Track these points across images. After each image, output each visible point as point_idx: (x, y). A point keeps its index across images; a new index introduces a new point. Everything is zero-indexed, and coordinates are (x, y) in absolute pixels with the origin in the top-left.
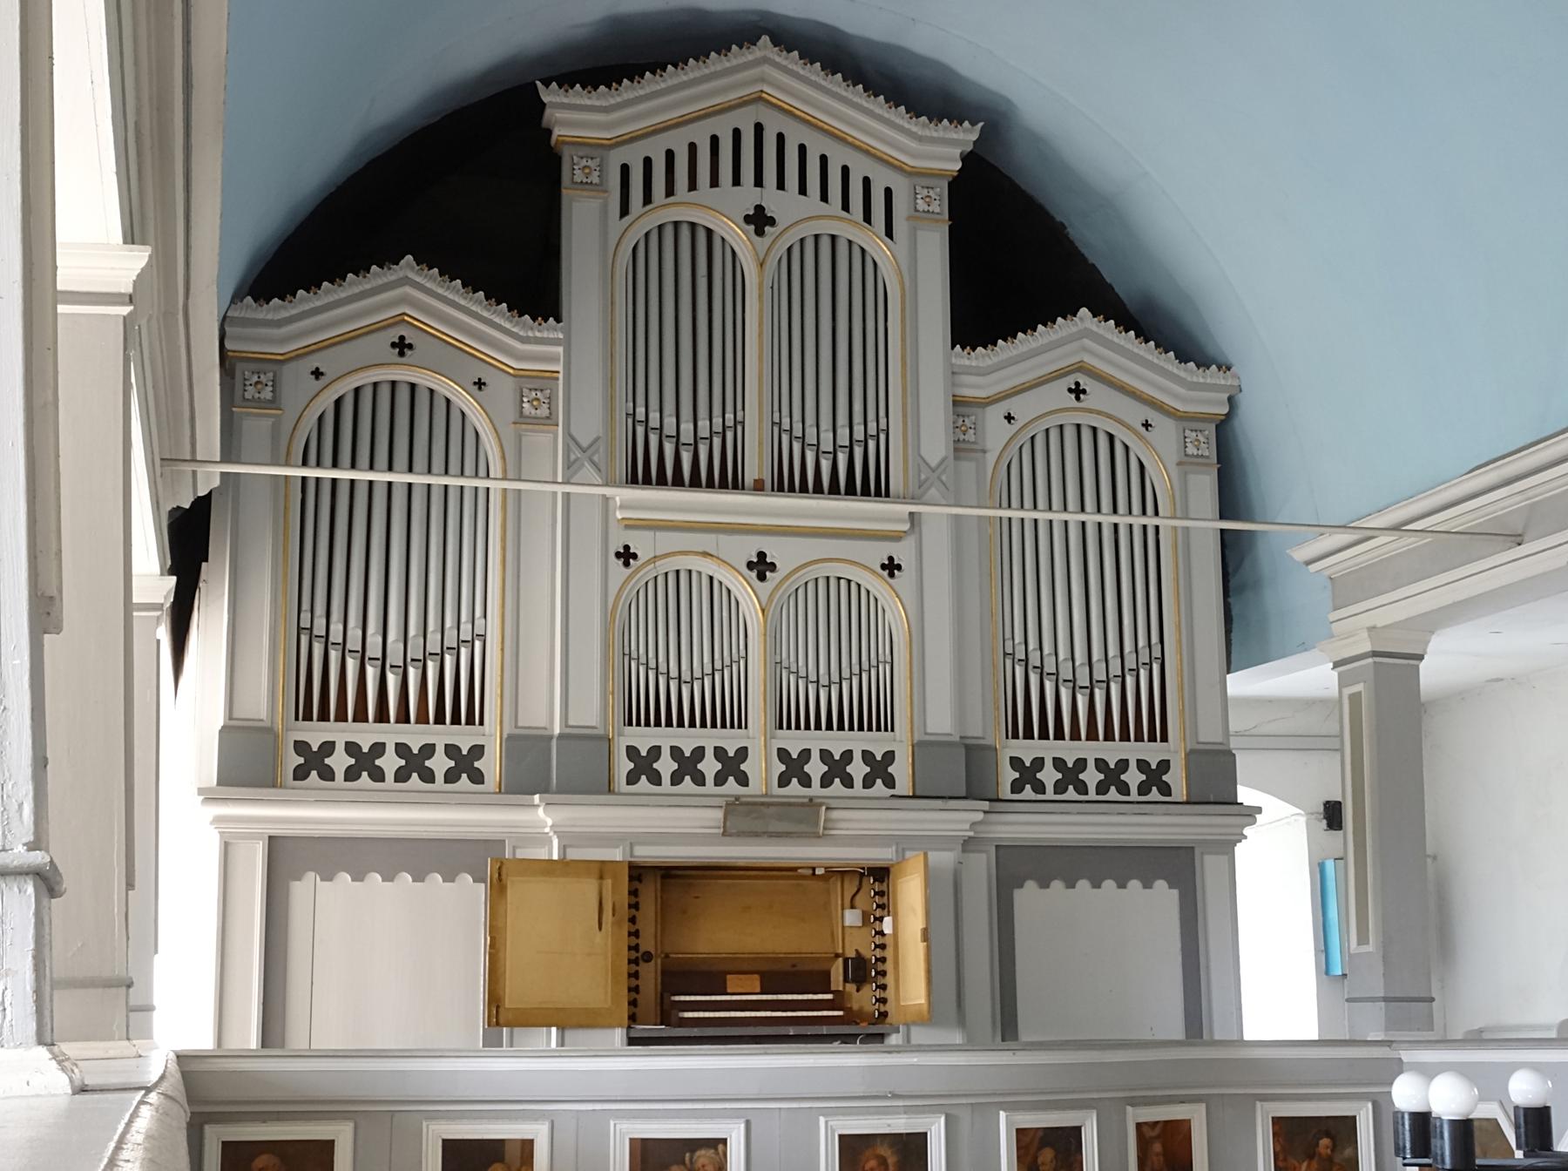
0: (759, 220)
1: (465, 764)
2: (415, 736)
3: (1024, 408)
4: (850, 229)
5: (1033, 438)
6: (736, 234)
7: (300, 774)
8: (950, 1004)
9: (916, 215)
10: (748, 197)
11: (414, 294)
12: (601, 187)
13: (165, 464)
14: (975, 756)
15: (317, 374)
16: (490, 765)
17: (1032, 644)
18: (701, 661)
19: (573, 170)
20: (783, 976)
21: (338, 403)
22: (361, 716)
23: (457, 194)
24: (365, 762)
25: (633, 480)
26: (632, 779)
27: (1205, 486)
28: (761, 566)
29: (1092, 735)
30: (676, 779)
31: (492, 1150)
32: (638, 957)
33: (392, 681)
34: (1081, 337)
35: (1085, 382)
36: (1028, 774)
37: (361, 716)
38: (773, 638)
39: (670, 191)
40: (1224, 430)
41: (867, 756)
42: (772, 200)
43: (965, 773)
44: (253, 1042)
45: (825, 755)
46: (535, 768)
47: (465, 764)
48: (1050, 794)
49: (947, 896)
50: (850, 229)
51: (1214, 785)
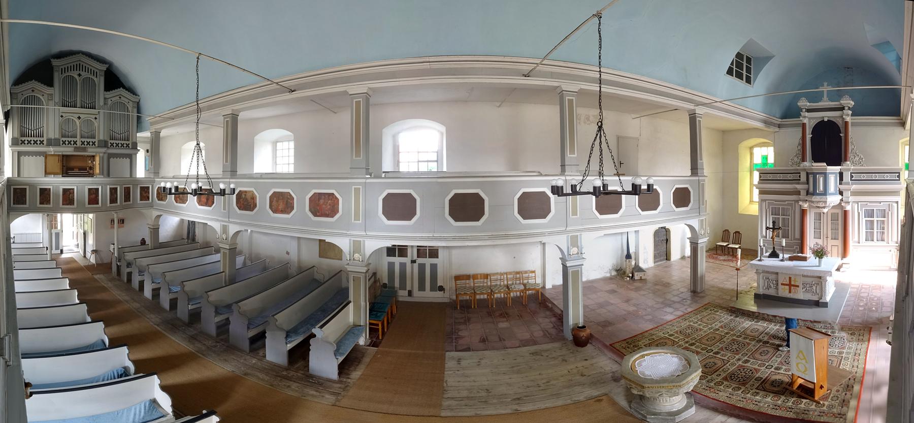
0: (79, 75)
1: (42, 142)
3: (113, 99)
6: (77, 77)
8: (102, 173)
10: (78, 72)
11: (34, 84)
13: (3, 106)
14: (106, 142)
16: (45, 142)
19: (55, 69)
20: (81, 169)
24: (29, 142)
27: (135, 110)
28: (79, 118)
31: (46, 189)
32: (63, 166)
34: (121, 91)
36: (112, 144)
40: (138, 103)
42: (81, 73)
43: (104, 144)
46: (50, 143)
49: (102, 159)
51: (135, 147)
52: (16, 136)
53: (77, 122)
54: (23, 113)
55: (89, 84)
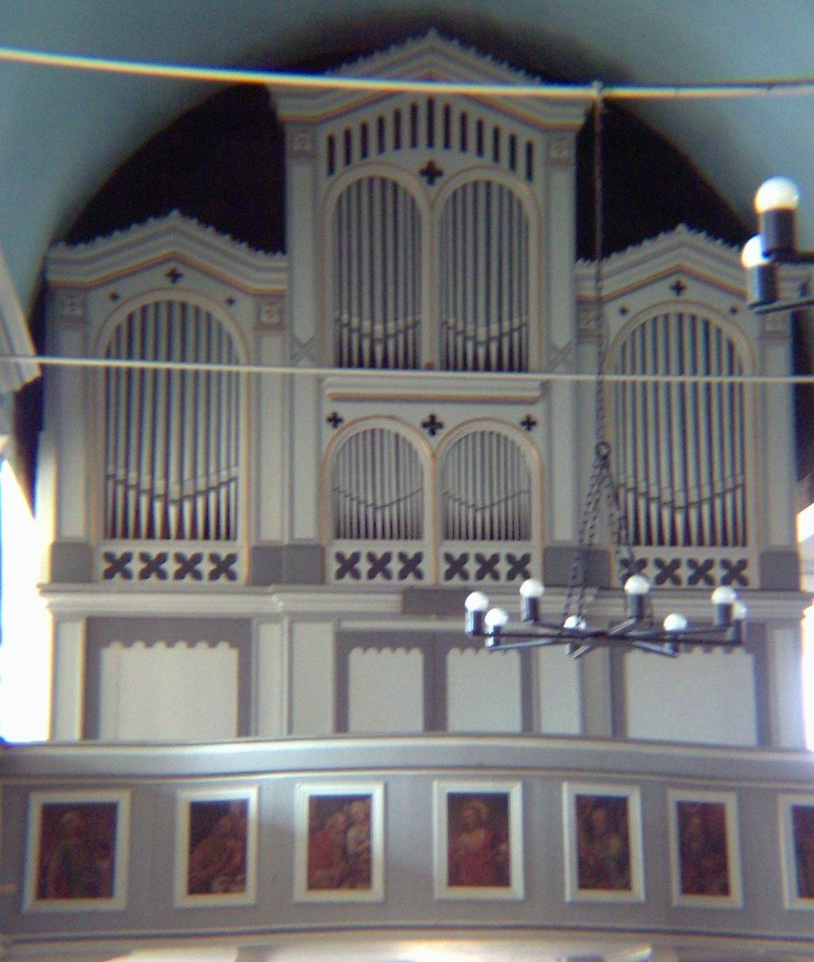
0: (431, 173)
1: (223, 567)
2: (188, 549)
3: (636, 303)
4: (501, 177)
5: (643, 326)
7: (109, 575)
9: (549, 162)
10: (421, 156)
11: (174, 234)
12: (313, 156)
14: (314, 552)
15: (114, 297)
16: (242, 567)
17: (641, 475)
18: (390, 495)
19: (295, 142)
21: (130, 318)
22: (151, 535)
23: (204, 167)
24: (153, 567)
25: (340, 364)
26: (340, 574)
28: (432, 425)
29: (688, 542)
30: (371, 575)
33: (173, 511)
34: (682, 246)
35: (685, 281)
37: (151, 535)
38: (442, 476)
39: (364, 154)
41: (510, 558)
42: (441, 157)
44: (76, 734)
45: (479, 558)
47: (223, 567)
48: (685, 585)
50: (501, 177)
52: (77, 529)
53: (423, 446)
54: (124, 404)
55: (487, 226)
